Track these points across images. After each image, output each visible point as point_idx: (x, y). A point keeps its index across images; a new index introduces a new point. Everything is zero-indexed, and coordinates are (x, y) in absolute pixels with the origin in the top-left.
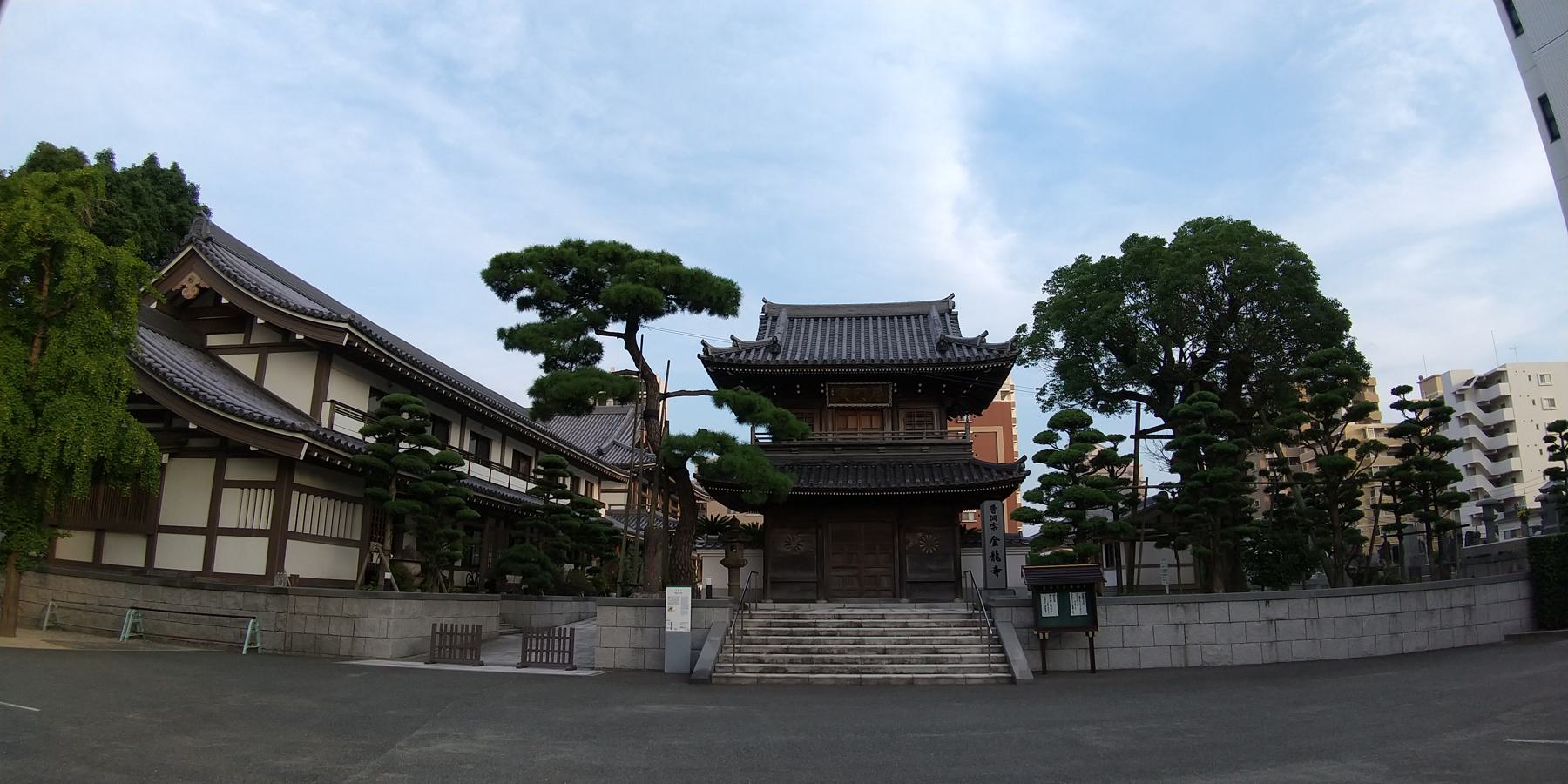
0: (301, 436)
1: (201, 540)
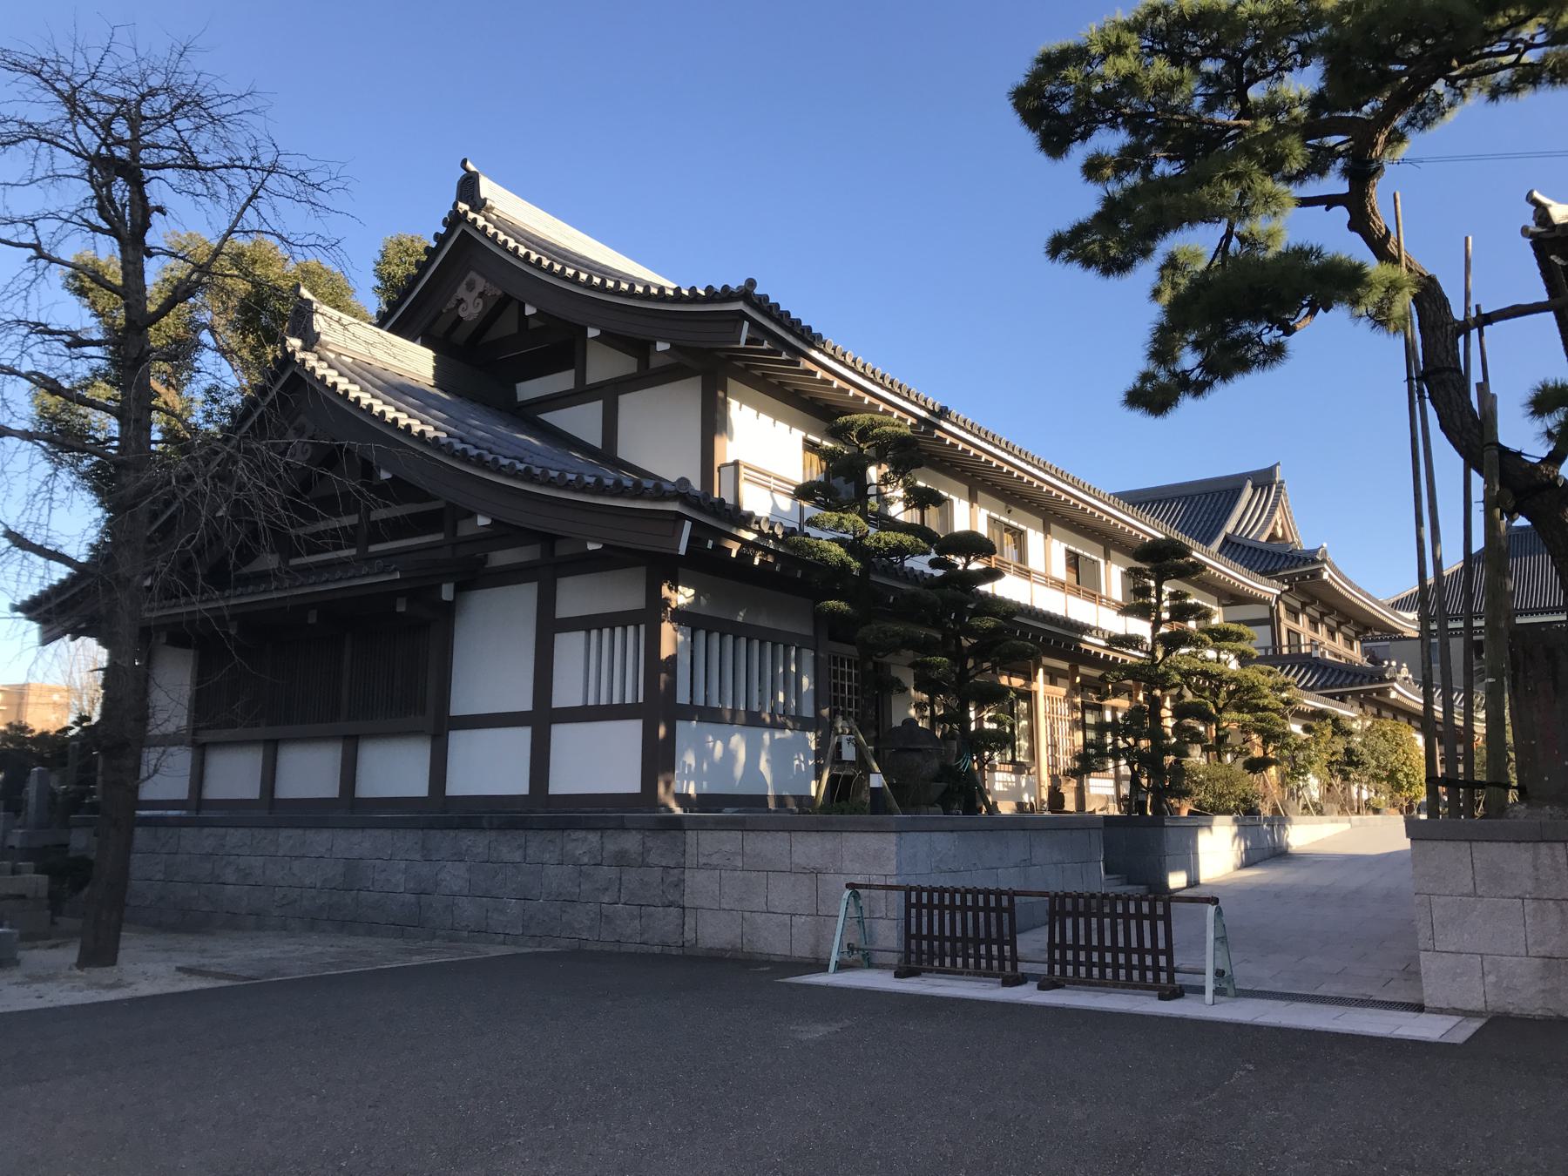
0: (674, 507)
1: (522, 737)
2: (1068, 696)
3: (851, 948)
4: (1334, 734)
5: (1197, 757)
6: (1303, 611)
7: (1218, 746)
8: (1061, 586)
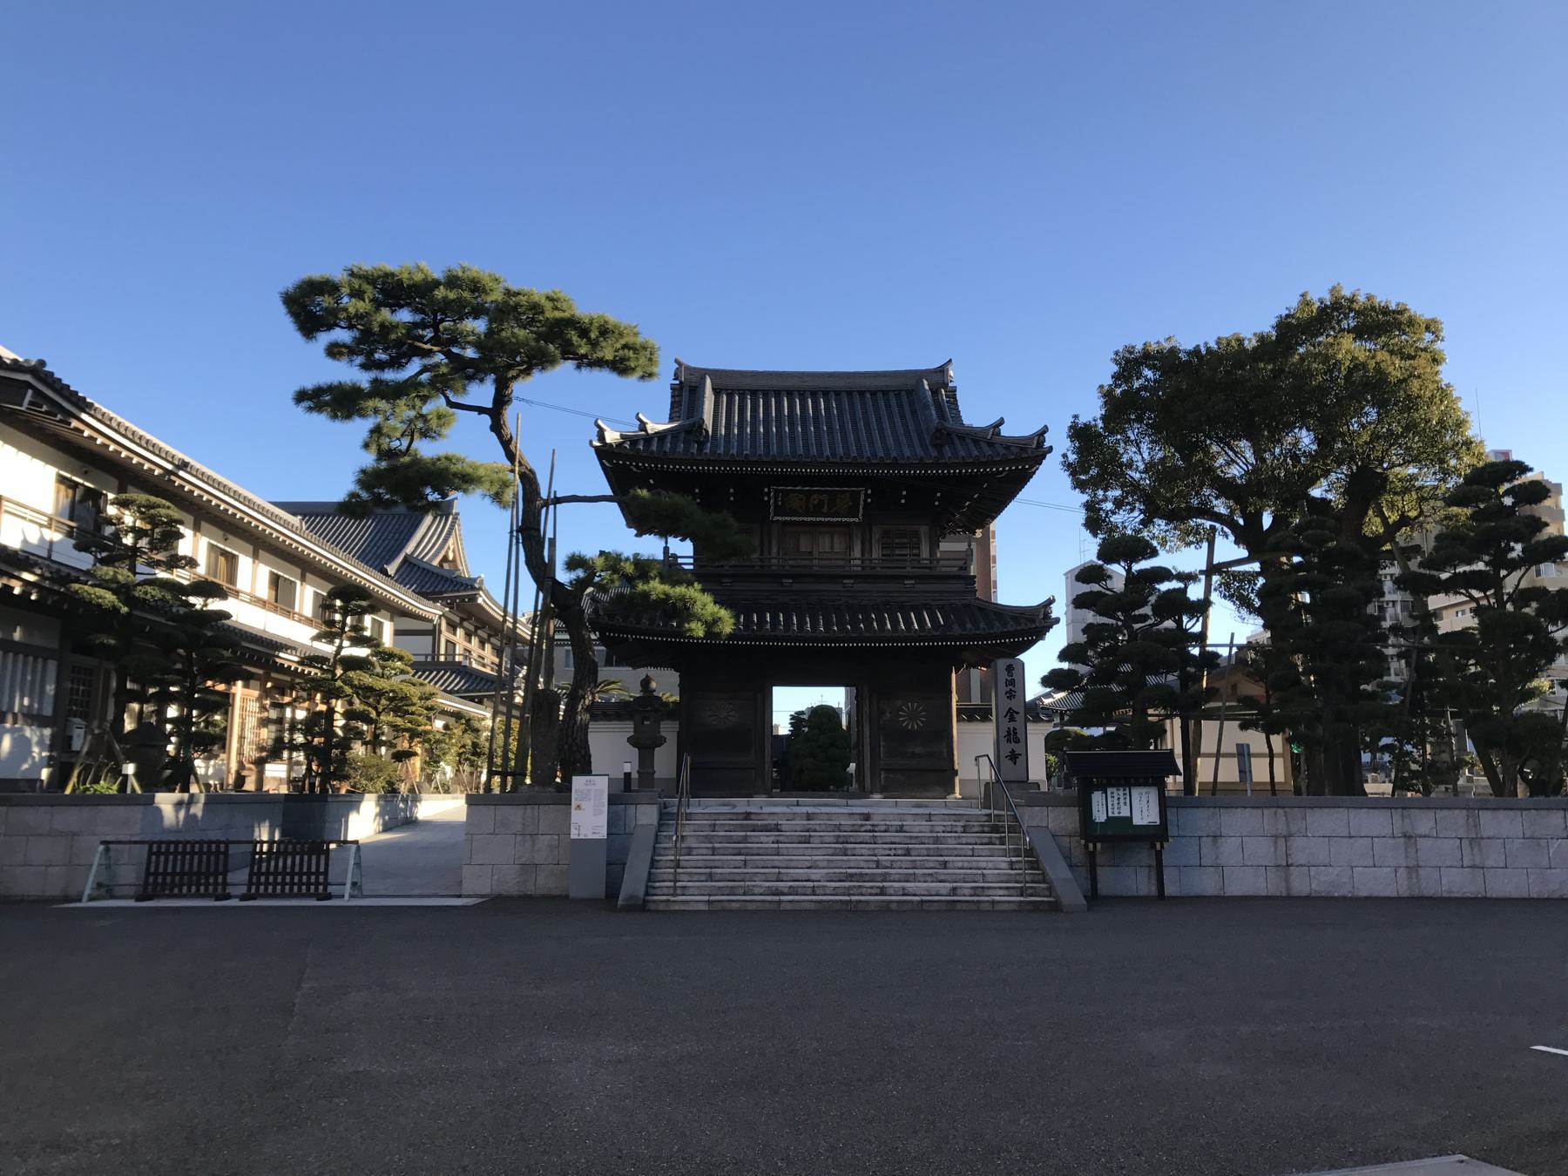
2: (259, 699)
3: (99, 885)
4: (465, 732)
5: (359, 749)
6: (461, 626)
7: (375, 743)
8: (262, 603)
